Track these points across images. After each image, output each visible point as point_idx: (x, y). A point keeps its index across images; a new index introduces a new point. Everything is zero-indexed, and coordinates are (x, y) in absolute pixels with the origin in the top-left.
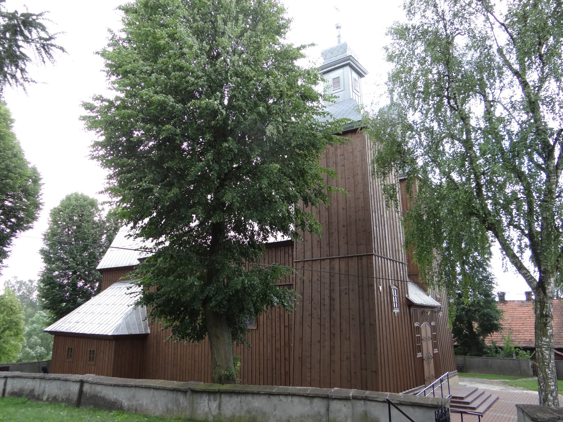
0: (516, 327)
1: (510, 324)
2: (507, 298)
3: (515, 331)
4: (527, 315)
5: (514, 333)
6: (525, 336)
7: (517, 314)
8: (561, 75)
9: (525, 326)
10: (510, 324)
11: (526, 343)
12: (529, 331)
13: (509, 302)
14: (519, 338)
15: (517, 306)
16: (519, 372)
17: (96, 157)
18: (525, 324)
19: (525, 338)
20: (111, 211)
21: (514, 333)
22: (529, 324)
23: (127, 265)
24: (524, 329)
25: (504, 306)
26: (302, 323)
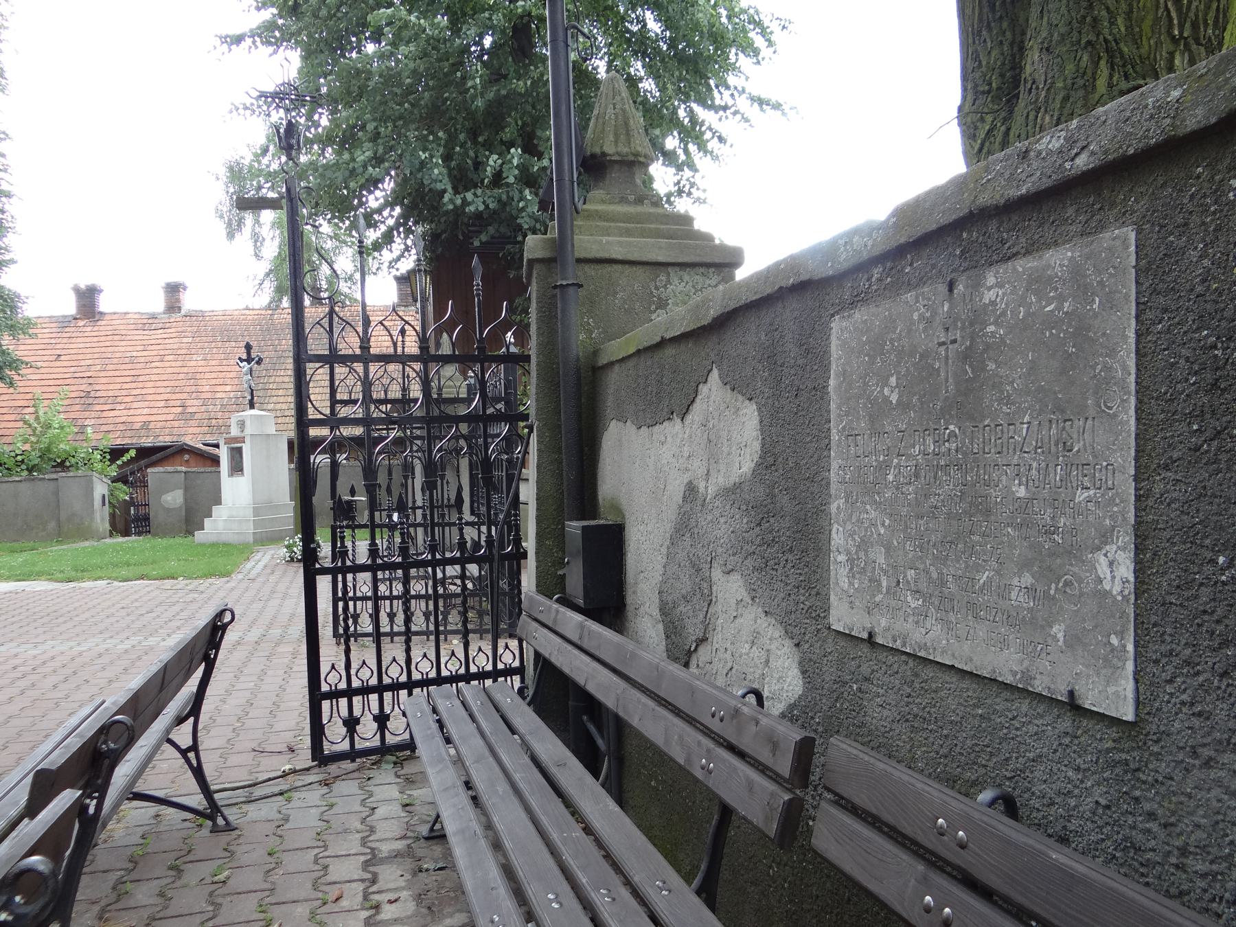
0: (111, 387)
1: (91, 380)
2: (105, 304)
3: (102, 401)
4: (155, 353)
5: (98, 408)
6: (131, 413)
7: (123, 349)
8: (1235, 866)
9: (141, 385)
10: (91, 380)
11: (129, 434)
12: (150, 398)
13: (107, 317)
14: (110, 421)
15: (132, 327)
16: (52, 525)
17: (769, 40)
18: (141, 379)
19: (130, 419)
20: (455, 177)
21: (98, 408)
22: (153, 378)
23: (566, 670)
24: (135, 392)
25: (89, 329)
26: (254, 622)
